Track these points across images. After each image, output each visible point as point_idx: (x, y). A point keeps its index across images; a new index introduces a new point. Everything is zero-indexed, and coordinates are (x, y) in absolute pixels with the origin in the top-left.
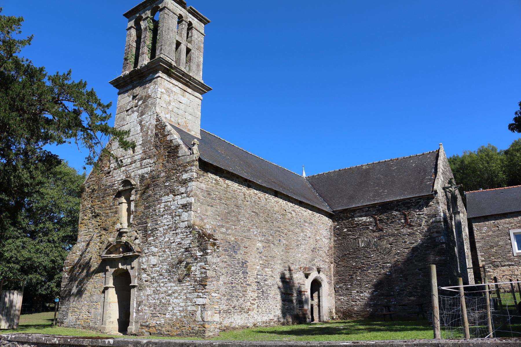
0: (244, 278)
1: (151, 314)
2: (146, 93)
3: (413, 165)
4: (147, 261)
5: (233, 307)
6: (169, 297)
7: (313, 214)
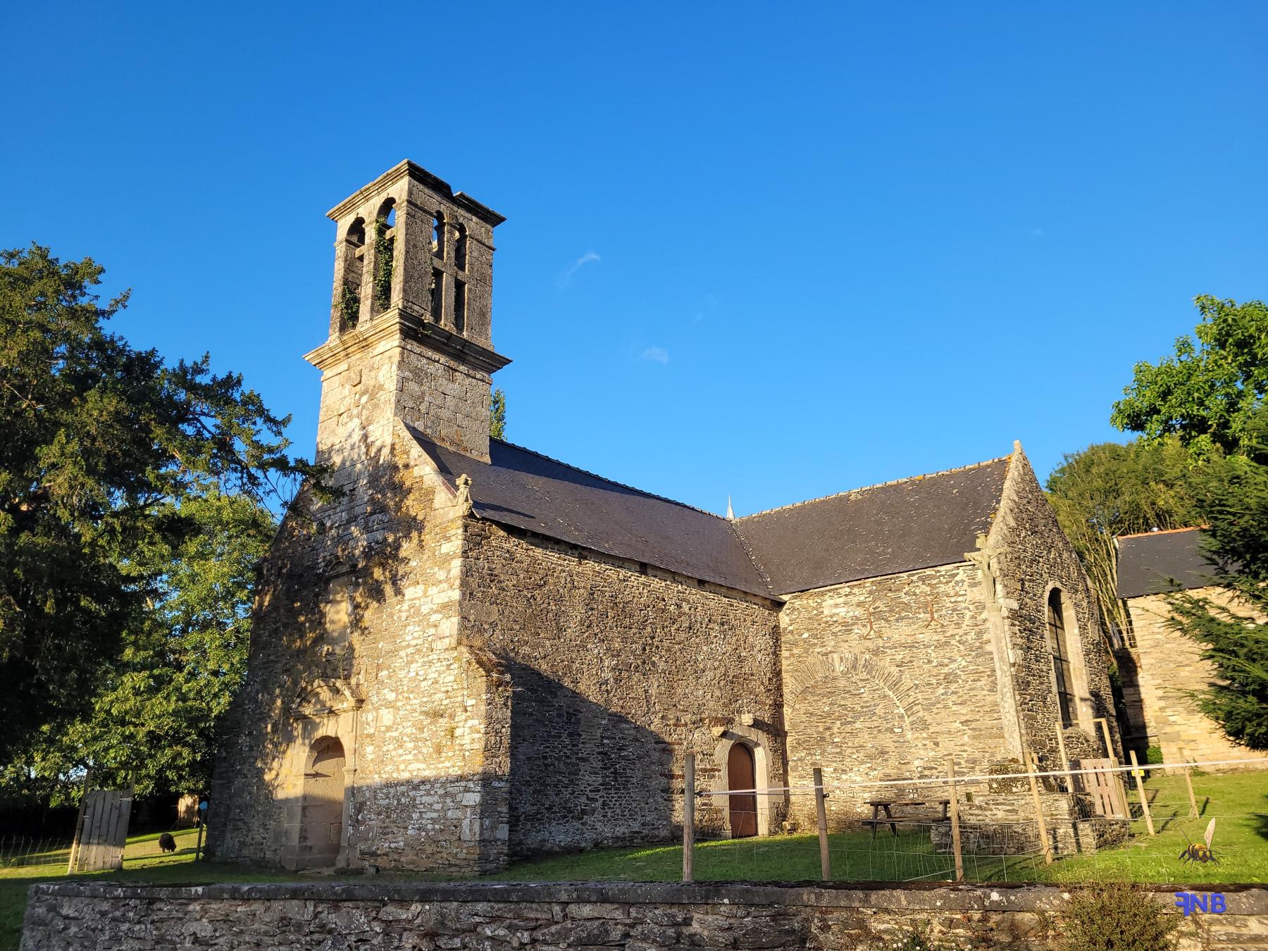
0: (573, 746)
1: (381, 827)
2: (374, 379)
3: (955, 491)
4: (377, 719)
5: (546, 809)
6: (414, 792)
7: (732, 605)
